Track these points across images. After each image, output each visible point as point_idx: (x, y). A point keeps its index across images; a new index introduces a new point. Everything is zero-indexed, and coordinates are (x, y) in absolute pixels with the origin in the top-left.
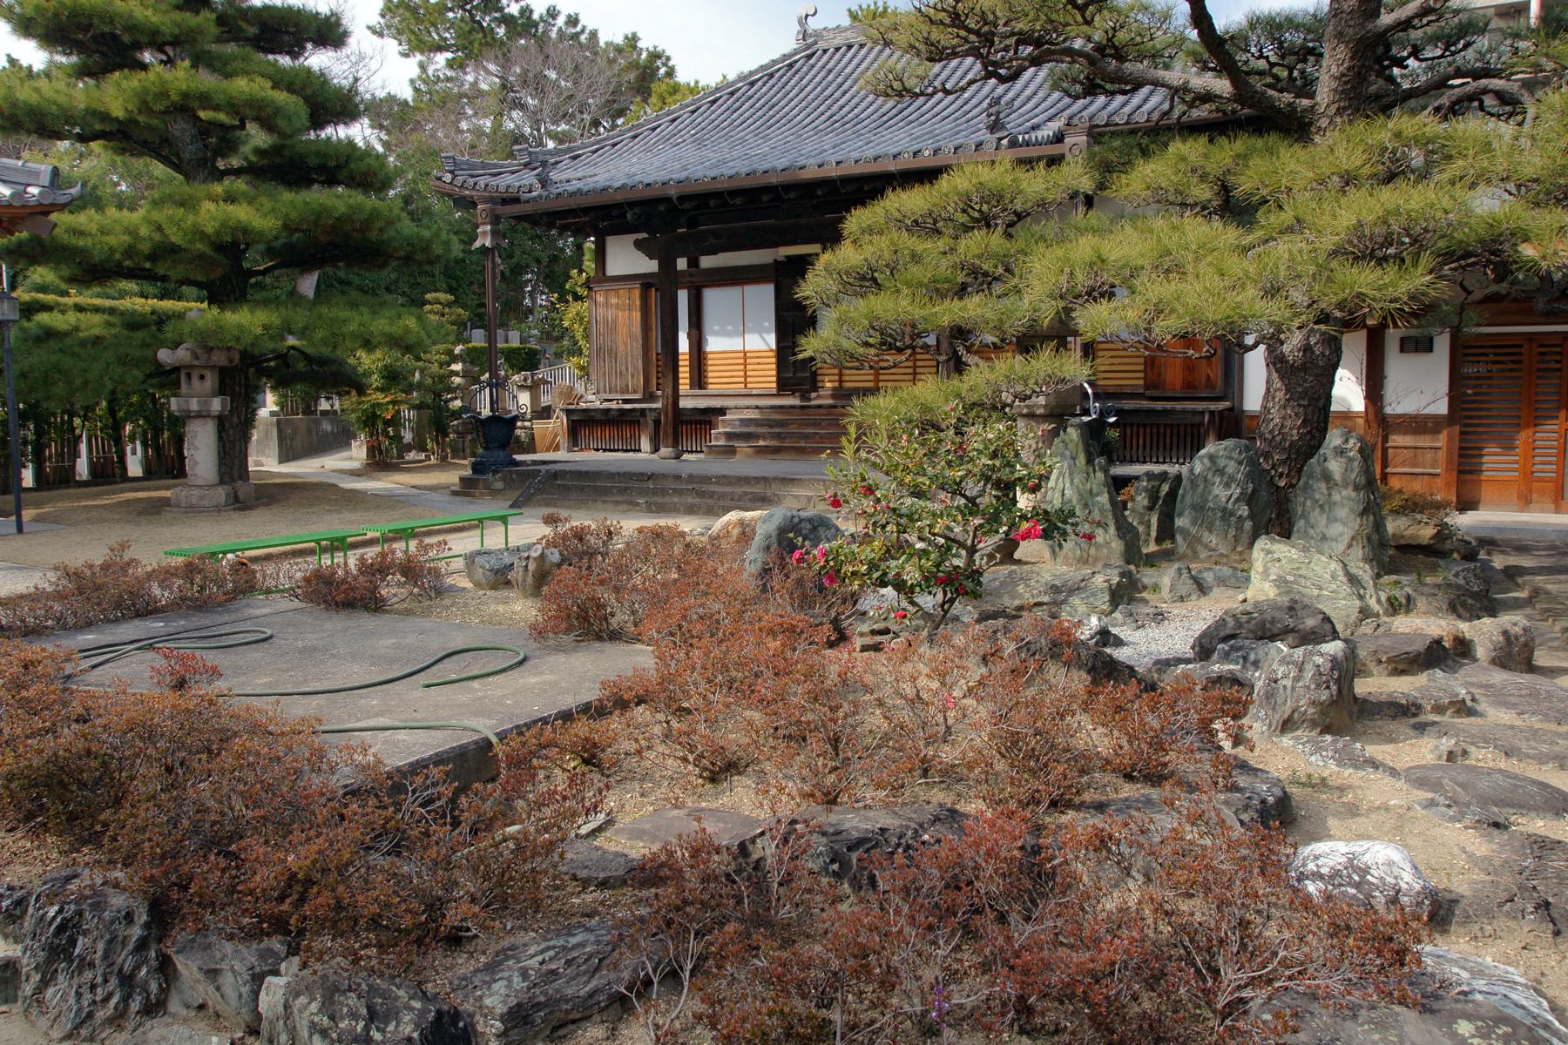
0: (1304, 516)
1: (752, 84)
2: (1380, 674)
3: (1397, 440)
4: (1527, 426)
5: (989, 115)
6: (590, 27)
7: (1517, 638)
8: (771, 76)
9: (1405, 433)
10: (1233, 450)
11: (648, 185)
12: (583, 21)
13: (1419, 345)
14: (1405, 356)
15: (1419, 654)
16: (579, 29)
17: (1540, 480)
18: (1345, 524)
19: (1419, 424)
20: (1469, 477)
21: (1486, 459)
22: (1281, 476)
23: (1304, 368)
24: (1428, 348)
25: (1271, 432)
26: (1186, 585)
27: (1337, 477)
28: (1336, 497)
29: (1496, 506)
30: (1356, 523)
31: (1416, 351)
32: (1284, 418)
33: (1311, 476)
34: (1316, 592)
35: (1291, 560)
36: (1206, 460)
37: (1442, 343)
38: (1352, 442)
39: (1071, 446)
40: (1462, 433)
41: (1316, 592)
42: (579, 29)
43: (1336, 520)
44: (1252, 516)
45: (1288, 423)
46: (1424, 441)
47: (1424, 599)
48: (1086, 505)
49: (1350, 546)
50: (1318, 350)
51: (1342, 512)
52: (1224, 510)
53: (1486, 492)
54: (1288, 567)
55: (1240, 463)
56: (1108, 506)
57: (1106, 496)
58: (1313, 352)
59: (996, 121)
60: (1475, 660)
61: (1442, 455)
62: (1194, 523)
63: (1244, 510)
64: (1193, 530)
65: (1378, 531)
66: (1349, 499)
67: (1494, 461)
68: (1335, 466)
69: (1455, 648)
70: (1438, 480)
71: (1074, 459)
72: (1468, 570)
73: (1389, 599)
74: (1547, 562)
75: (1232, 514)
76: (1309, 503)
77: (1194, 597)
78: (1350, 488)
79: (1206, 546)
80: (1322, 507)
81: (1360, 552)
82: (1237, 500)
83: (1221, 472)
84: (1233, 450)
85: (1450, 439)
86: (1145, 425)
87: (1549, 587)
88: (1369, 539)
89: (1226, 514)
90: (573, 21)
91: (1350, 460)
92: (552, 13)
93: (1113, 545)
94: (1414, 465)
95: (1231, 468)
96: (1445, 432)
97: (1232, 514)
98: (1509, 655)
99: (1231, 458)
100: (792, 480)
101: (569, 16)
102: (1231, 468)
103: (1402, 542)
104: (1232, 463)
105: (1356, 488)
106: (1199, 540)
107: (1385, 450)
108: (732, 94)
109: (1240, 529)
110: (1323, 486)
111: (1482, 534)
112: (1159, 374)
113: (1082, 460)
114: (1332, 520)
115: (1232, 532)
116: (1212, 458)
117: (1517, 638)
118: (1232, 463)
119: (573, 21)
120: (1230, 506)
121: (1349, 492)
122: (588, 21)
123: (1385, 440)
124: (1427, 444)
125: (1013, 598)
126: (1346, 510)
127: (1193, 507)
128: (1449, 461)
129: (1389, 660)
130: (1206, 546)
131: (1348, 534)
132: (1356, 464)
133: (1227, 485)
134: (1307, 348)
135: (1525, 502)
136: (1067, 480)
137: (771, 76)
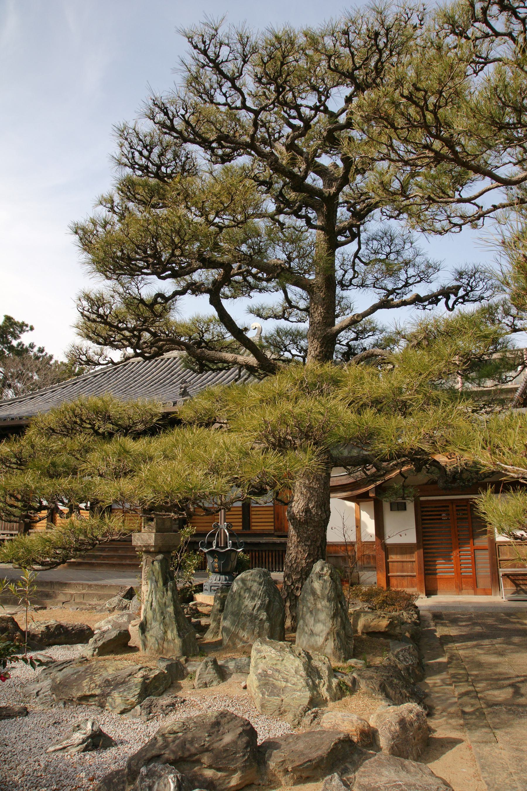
0: (303, 618)
1: (96, 376)
2: (287, 784)
3: (393, 558)
4: (456, 548)
5: (181, 388)
6: (49, 353)
7: (411, 724)
8: (105, 373)
9: (396, 554)
10: (256, 575)
11: (13, 419)
12: (46, 350)
13: (401, 507)
14: (393, 512)
15: (321, 759)
16: (44, 354)
17: (466, 577)
18: (324, 624)
19: (403, 549)
20: (431, 577)
21: (438, 566)
22: (297, 589)
23: (306, 522)
24: (405, 509)
25: (291, 561)
26: (211, 674)
27: (319, 592)
28: (319, 606)
29: (445, 592)
30: (329, 624)
31: (398, 510)
32: (297, 553)
33: (306, 592)
34: (284, 684)
35: (272, 658)
36: (240, 583)
37: (411, 507)
38: (325, 569)
39: (156, 574)
40: (424, 553)
41: (284, 684)
42: (44, 354)
43: (319, 621)
44: (269, 619)
45: (300, 556)
46: (406, 558)
47: (364, 681)
48: (162, 613)
49: (326, 639)
50: (314, 511)
51: (323, 616)
52: (251, 615)
53: (440, 585)
54: (270, 662)
55: (260, 584)
56: (173, 615)
57: (172, 607)
58: (311, 513)
59: (185, 391)
60: (379, 749)
61: (415, 565)
62: (233, 623)
63: (263, 615)
64: (233, 629)
65: (344, 628)
66: (326, 607)
67: (443, 568)
68: (317, 585)
69: (362, 740)
70: (415, 579)
71: (157, 582)
72: (405, 650)
73: (339, 684)
74: (465, 631)
75: (256, 618)
76: (305, 609)
77: (215, 683)
78: (326, 600)
79: (241, 640)
80: (311, 612)
81: (333, 644)
82: (259, 609)
83: (249, 590)
84: (256, 575)
85: (419, 557)
86: (272, 551)
87: (461, 652)
88: (338, 634)
89: (253, 618)
90: (41, 350)
91: (325, 581)
92: (32, 346)
93: (176, 641)
94: (402, 571)
95: (255, 587)
96: (416, 553)
97: (256, 618)
98: (406, 741)
99: (255, 581)
100: (66, 584)
101: (40, 348)
102: (255, 587)
103: (370, 630)
104: (255, 584)
105: (329, 600)
106: (237, 635)
107: (387, 564)
108: (85, 380)
109: (261, 628)
110: (312, 598)
111: (436, 610)
112: (281, 523)
113: (161, 583)
114: (317, 621)
115: (257, 630)
116: (243, 581)
117: (411, 724)
118: (255, 584)
119: (41, 350)
120: (255, 612)
121: (325, 603)
122: (49, 351)
123: (387, 558)
124: (408, 560)
125: (78, 690)
126: (325, 614)
127: (232, 614)
128: (419, 569)
129: (294, 770)
130: (241, 640)
131: (326, 630)
132: (328, 584)
133: (253, 598)
134: (307, 511)
135: (460, 590)
136: (154, 596)
137: (105, 373)
